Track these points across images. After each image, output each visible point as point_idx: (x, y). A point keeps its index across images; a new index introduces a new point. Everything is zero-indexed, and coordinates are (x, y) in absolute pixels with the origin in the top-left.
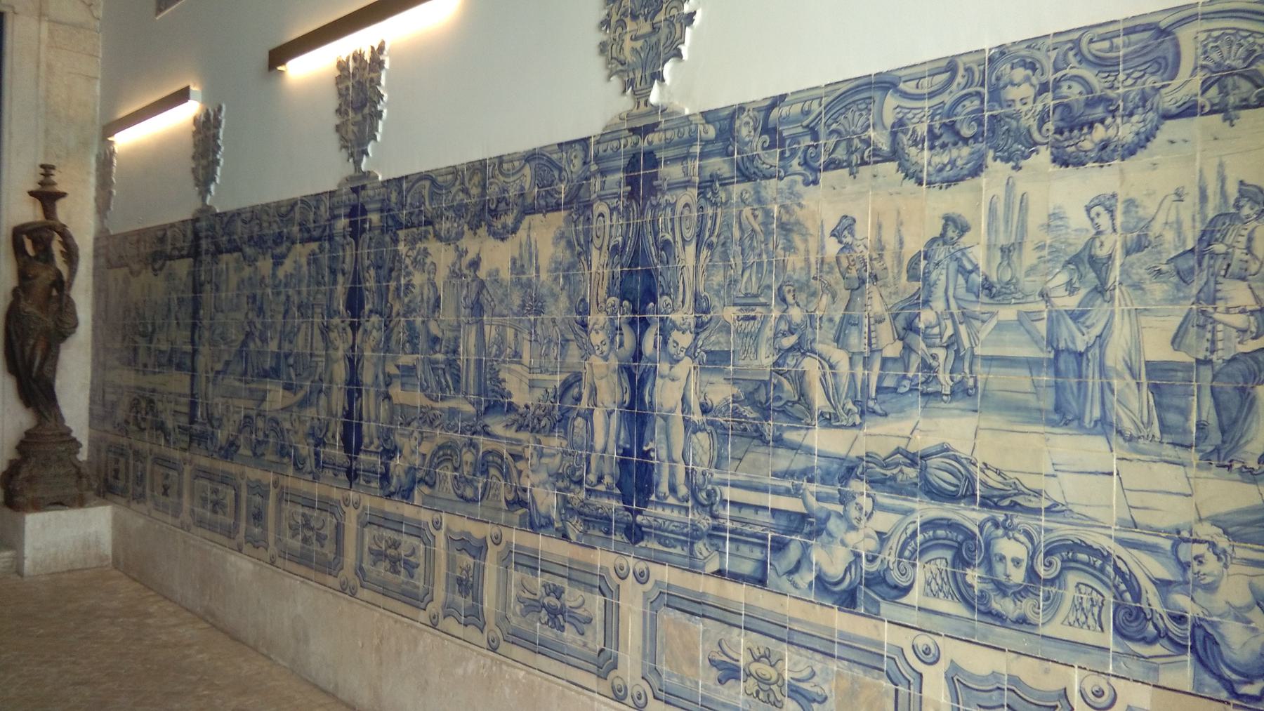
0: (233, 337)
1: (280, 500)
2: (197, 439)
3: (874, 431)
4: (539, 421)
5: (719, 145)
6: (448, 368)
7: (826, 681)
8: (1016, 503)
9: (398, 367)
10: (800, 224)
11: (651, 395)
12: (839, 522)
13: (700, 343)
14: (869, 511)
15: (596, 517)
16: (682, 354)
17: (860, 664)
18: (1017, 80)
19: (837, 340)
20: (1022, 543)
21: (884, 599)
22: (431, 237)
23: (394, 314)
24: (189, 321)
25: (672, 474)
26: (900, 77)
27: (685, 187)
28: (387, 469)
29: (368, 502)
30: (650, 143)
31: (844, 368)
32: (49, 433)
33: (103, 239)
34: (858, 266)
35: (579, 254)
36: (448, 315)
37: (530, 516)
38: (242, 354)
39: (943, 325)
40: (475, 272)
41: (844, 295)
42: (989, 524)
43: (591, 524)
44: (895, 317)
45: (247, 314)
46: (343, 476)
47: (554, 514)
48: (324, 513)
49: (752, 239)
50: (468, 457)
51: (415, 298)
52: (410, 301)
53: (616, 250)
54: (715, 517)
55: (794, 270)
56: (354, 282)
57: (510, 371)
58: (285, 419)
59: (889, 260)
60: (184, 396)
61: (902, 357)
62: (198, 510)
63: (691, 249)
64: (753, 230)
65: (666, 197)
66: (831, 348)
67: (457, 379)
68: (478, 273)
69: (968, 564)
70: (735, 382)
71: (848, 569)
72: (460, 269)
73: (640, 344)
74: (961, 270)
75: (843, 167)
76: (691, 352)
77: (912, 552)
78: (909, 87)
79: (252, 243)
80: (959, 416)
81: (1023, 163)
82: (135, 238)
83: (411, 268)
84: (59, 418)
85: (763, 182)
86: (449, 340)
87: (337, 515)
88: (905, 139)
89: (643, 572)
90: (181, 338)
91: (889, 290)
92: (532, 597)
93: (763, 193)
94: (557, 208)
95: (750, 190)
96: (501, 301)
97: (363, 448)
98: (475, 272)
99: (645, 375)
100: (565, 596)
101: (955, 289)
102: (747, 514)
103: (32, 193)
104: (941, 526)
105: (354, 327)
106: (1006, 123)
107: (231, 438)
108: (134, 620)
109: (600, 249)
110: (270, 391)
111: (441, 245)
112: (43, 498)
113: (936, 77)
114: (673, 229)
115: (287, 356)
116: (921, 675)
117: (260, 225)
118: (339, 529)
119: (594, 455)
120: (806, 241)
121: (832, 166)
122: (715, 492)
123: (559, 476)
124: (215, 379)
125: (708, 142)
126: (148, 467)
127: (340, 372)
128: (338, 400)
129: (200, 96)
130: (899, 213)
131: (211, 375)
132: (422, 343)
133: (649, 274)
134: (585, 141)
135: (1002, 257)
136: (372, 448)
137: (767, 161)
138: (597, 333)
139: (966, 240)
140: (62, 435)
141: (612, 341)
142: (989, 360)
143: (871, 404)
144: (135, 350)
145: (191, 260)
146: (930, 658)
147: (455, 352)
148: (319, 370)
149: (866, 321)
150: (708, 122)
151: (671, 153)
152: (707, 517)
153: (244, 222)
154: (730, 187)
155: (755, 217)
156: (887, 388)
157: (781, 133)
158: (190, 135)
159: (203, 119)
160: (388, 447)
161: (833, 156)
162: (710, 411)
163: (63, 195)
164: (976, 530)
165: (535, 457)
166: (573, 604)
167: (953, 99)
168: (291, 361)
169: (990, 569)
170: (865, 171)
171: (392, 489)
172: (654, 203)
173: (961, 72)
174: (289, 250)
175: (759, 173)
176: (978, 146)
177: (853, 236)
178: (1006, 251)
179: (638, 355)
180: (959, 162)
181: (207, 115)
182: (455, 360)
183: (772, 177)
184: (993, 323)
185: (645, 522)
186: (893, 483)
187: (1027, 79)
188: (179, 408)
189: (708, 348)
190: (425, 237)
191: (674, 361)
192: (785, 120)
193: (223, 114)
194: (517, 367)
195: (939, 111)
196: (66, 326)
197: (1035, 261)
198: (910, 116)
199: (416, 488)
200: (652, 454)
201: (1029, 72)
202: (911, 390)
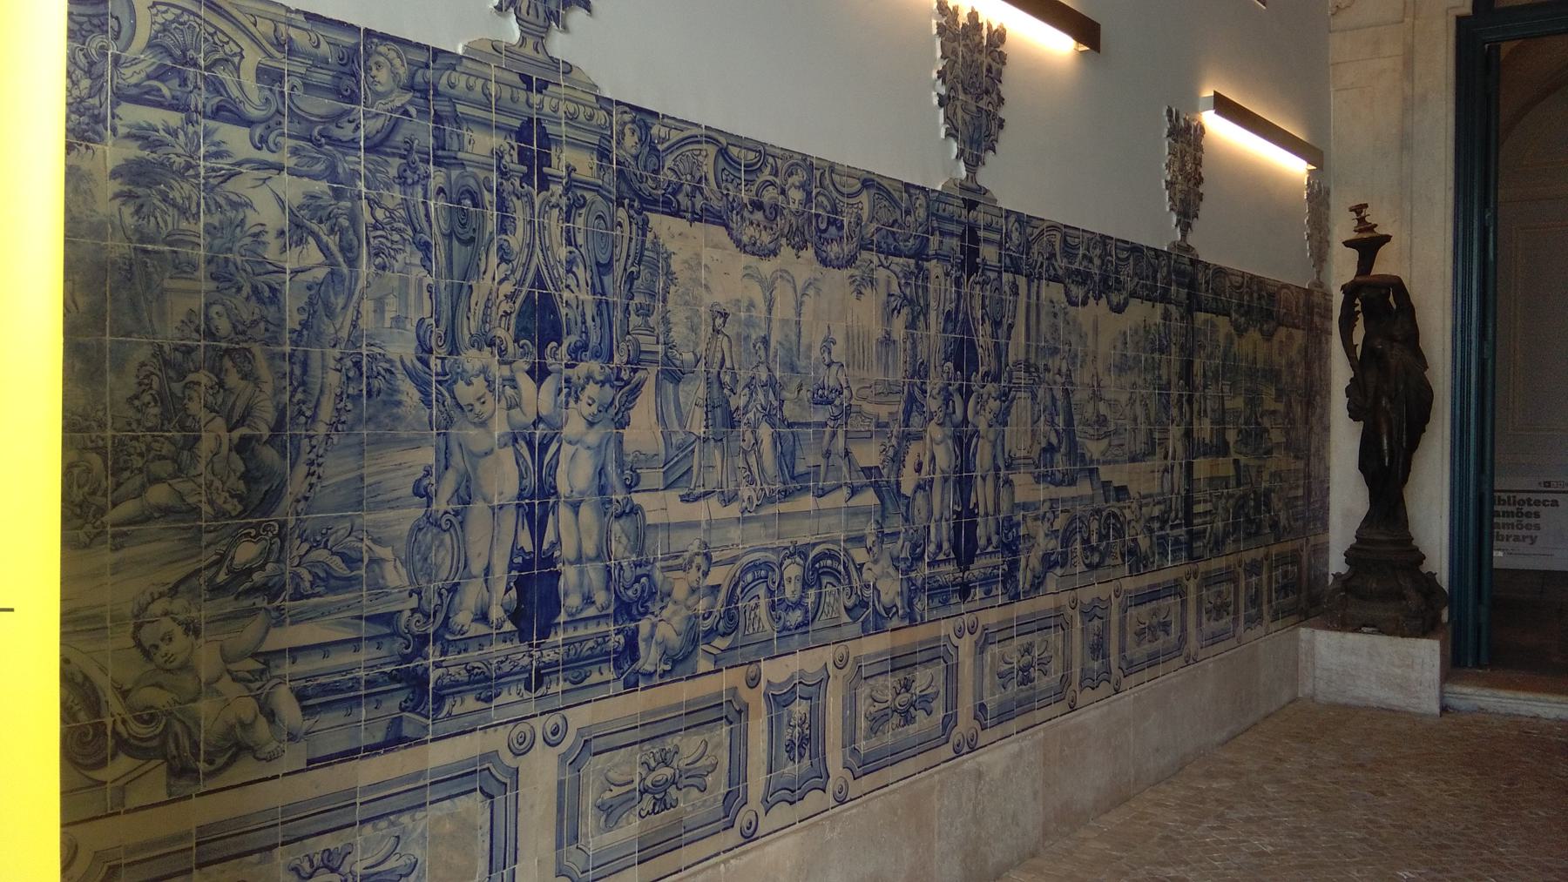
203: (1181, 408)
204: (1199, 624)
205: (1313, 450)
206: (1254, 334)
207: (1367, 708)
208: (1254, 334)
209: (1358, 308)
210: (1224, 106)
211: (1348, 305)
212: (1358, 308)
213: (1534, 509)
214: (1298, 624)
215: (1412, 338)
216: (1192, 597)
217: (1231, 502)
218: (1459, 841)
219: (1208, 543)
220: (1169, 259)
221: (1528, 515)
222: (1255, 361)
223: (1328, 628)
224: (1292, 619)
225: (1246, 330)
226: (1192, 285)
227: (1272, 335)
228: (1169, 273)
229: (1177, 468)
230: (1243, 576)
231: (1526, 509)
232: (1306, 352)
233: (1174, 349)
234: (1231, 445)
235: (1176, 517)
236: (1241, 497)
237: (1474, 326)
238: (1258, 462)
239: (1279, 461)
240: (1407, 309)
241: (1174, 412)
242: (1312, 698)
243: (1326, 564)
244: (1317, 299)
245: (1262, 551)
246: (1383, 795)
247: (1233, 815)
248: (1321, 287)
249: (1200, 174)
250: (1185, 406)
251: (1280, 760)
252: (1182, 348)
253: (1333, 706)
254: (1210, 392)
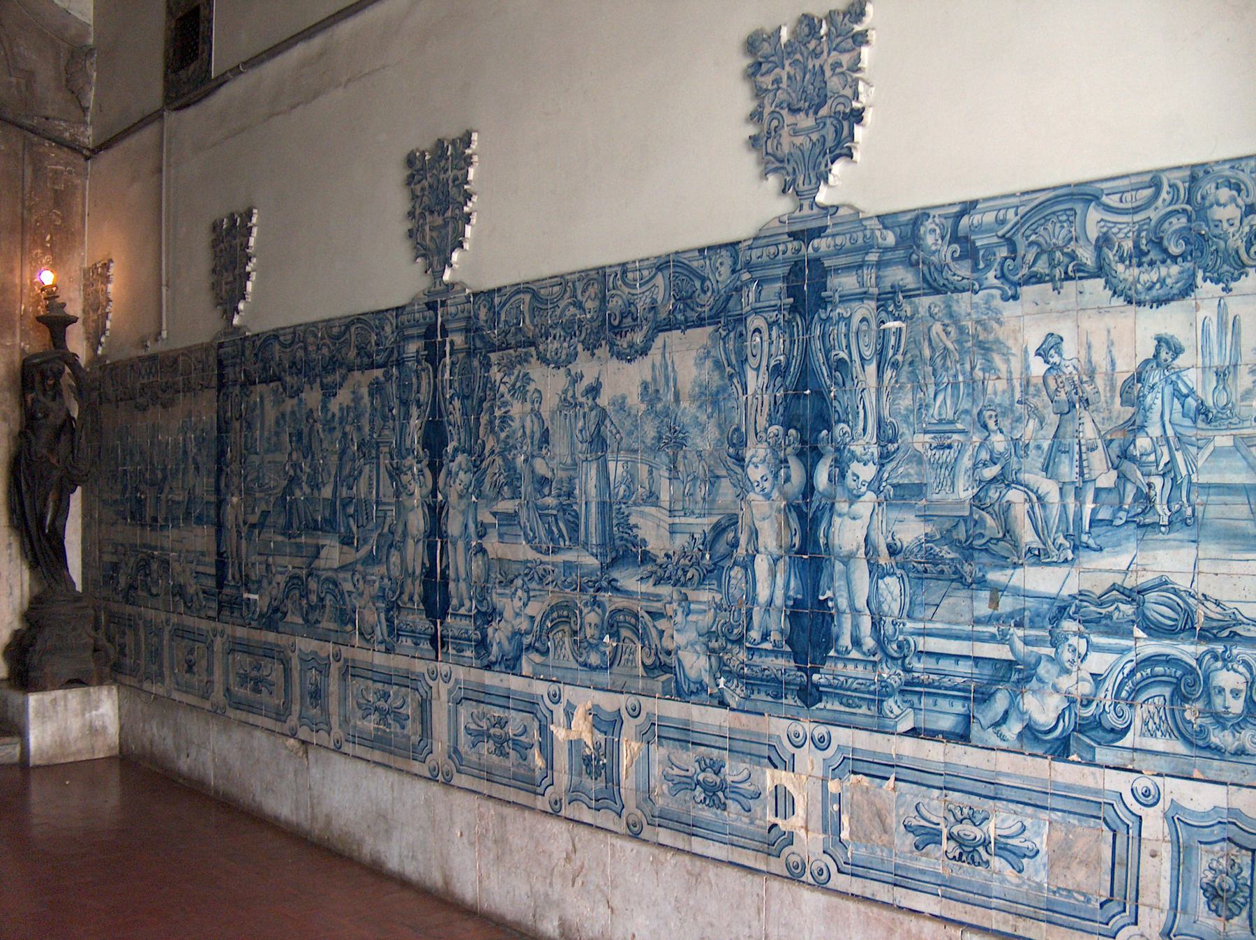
0: (272, 484)
1: (344, 675)
2: (230, 606)
3: (1093, 566)
4: (685, 572)
5: (901, 253)
6: (561, 514)
7: (1038, 834)
8: (1236, 634)
9: (494, 514)
10: (1001, 343)
11: (827, 537)
12: (1049, 666)
13: (886, 475)
14: (1083, 653)
15: (762, 680)
16: (864, 489)
17: (1075, 813)
18: (1222, 201)
19: (1046, 469)
20: (1241, 674)
21: (1099, 744)
22: (533, 360)
23: (487, 452)
25: (856, 626)
26: (1102, 190)
27: (862, 300)
28: (485, 636)
29: (460, 673)
30: (816, 250)
31: (1054, 497)
34: (1067, 388)
35: (731, 376)
36: (560, 447)
37: (676, 681)
38: (285, 503)
39: (1159, 453)
40: (594, 399)
41: (1053, 419)
42: (1208, 657)
43: (755, 688)
44: (1108, 444)
45: (290, 454)
46: (426, 645)
47: (707, 679)
48: (403, 689)
49: (944, 358)
50: (592, 617)
51: (514, 432)
52: (508, 437)
53: (777, 371)
54: (907, 671)
55: (995, 393)
56: (432, 414)
57: (642, 514)
58: (345, 580)
59: (1100, 381)
61: (1116, 487)
63: (872, 368)
64: (946, 348)
65: (838, 310)
66: (1039, 478)
67: (574, 527)
68: (598, 400)
69: (1185, 699)
70: (926, 518)
71: (1060, 716)
72: (573, 396)
73: (812, 477)
74: (1177, 394)
75: (1045, 282)
76: (875, 485)
77: (1131, 691)
78: (1113, 201)
79: (294, 370)
80: (1178, 547)
81: (1232, 285)
83: (508, 397)
85: (955, 296)
86: (561, 481)
87: (421, 690)
88: (1111, 255)
89: (823, 737)
90: (203, 485)
91: (1101, 415)
92: (683, 773)
93: (955, 308)
94: (700, 322)
95: (939, 303)
96: (630, 433)
97: (450, 611)
98: (594, 399)
99: (819, 513)
100: (726, 769)
101: (1171, 414)
102: (946, 665)
104: (1158, 663)
105: (435, 469)
106: (1217, 244)
107: (275, 604)
109: (757, 369)
110: (323, 546)
111: (550, 370)
113: (1140, 191)
114: (848, 347)
115: (344, 506)
116: (1140, 817)
117: (305, 349)
118: (425, 706)
119: (756, 609)
120: (1008, 361)
121: (1033, 280)
122: (908, 643)
123: (710, 634)
124: (250, 533)
125: (886, 249)
127: (417, 522)
128: (415, 554)
130: (1109, 331)
131: (245, 530)
132: (526, 487)
133: (820, 395)
134: (734, 245)
135: (1218, 381)
136: (462, 611)
137: (958, 272)
138: (757, 467)
139: (1181, 361)
141: (776, 476)
142: (1207, 487)
143: (1084, 538)
146: (1150, 800)
147: (570, 494)
148: (388, 520)
149: (1077, 448)
150: (885, 228)
151: (842, 261)
152: (899, 671)
153: (283, 345)
154: (916, 300)
155: (948, 334)
156: (1102, 520)
157: (974, 243)
160: (484, 609)
161: (1034, 269)
162: (900, 552)
164: (1194, 663)
165: (680, 613)
166: (736, 779)
167: (1158, 216)
168: (351, 510)
169: (1209, 702)
170: (1070, 286)
171: (493, 658)
172: (823, 316)
173: (1166, 188)
174: (344, 378)
175: (950, 286)
176: (1188, 265)
177: (1060, 355)
178: (1221, 375)
179: (809, 488)
180: (1169, 281)
182: (570, 505)
183: (964, 290)
184: (1211, 447)
185: (822, 681)
186: (1108, 621)
187: (1233, 200)
188: (201, 569)
189: (895, 481)
190: (526, 361)
191: (854, 498)
192: (979, 229)
194: (653, 510)
195: (1145, 227)
197: (1251, 386)
198: (1115, 230)
199: (524, 658)
200: (830, 604)
201: (1235, 193)
202: (1127, 522)
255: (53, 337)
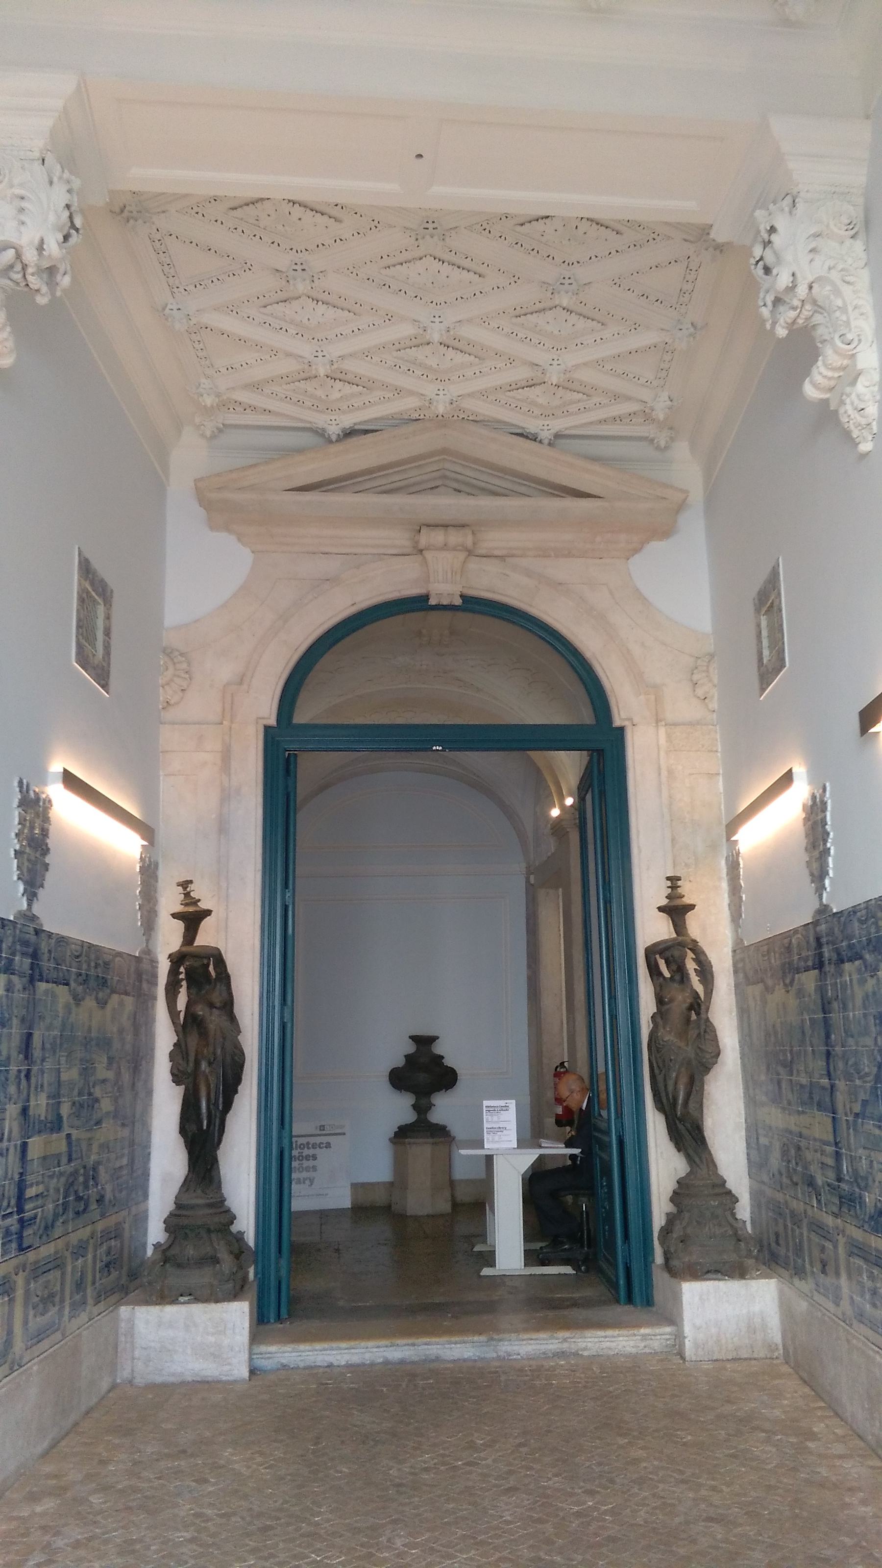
0: (867, 1070)
24: (823, 1048)
32: (701, 1183)
33: (739, 950)
60: (827, 1143)
62: (857, 1299)
79: (871, 948)
82: (765, 948)
84: (711, 1164)
103: (660, 909)
108: (793, 1440)
112: (700, 1264)
126: (805, 1233)
129: (805, 776)
131: (851, 1118)
140: (714, 1186)
144: (779, 1083)
145: (817, 971)
158: (801, 823)
159: (810, 803)
163: (692, 907)
181: (814, 797)
193: (828, 794)
196: (708, 1056)
203: (19, 1084)
204: (26, 1322)
205: (137, 1116)
206: (90, 1003)
207: (183, 1383)
208: (90, 1003)
209: (182, 976)
210: (70, 780)
211: (173, 972)
212: (182, 976)
213: (311, 1152)
214: (118, 1303)
215: (228, 1006)
216: (20, 1293)
217: (63, 1180)
218: (278, 1519)
219: (38, 1230)
220: (15, 928)
221: (307, 1158)
222: (89, 1030)
223: (147, 1303)
224: (113, 1299)
225: (83, 999)
226: (35, 956)
227: (106, 1003)
228: (14, 942)
229: (12, 1150)
230: (69, 1260)
231: (306, 1152)
232: (135, 1018)
233: (15, 1021)
234: (65, 1119)
235: (9, 1206)
236: (71, 1174)
237: (277, 993)
238: (88, 1135)
239: (108, 1131)
240: (224, 977)
241: (12, 1089)
242: (131, 1382)
243: (145, 1234)
244: (145, 966)
245: (88, 1229)
246: (206, 1481)
247: (60, 1543)
248: (149, 955)
249: (47, 844)
250: (24, 1082)
251: (103, 1462)
252: (23, 1020)
253: (152, 1387)
254: (47, 1065)
255: (675, 926)
